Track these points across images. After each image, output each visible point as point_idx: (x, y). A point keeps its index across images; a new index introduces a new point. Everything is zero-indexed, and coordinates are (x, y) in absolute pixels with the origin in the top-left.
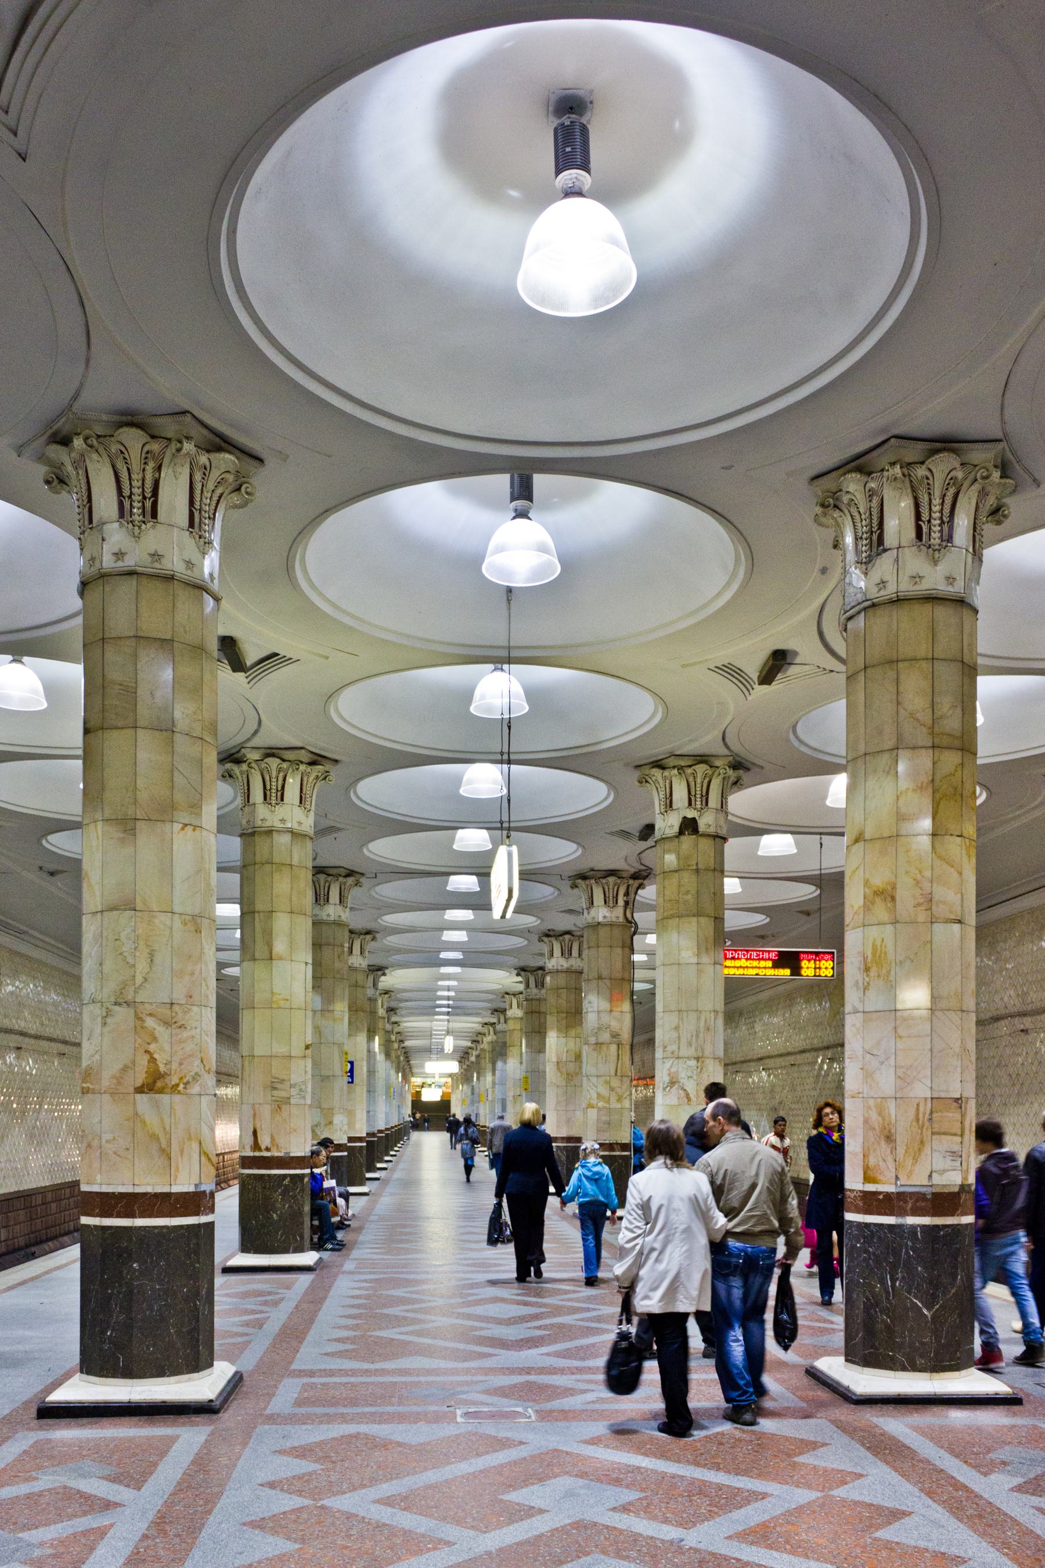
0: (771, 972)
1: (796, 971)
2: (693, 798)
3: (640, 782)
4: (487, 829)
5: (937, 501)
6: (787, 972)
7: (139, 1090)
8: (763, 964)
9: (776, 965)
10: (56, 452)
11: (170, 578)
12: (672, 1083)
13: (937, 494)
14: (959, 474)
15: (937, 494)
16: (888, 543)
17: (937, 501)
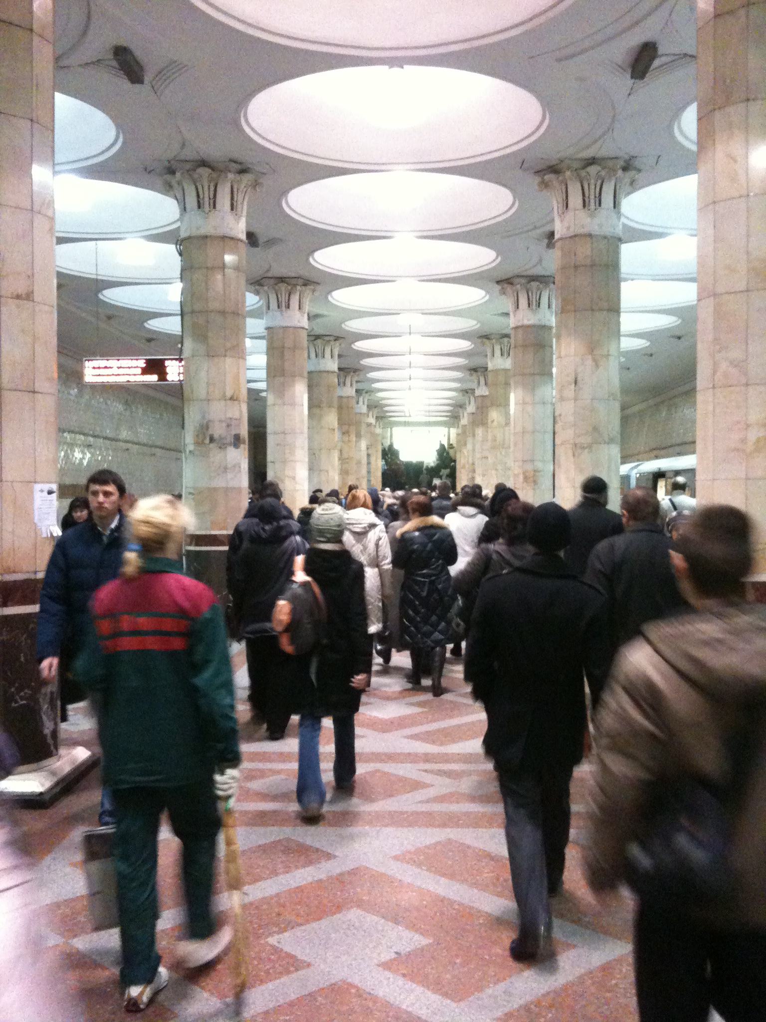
2: (587, 200)
5: (592, 187)
10: (168, 177)
14: (603, 173)
17: (592, 187)
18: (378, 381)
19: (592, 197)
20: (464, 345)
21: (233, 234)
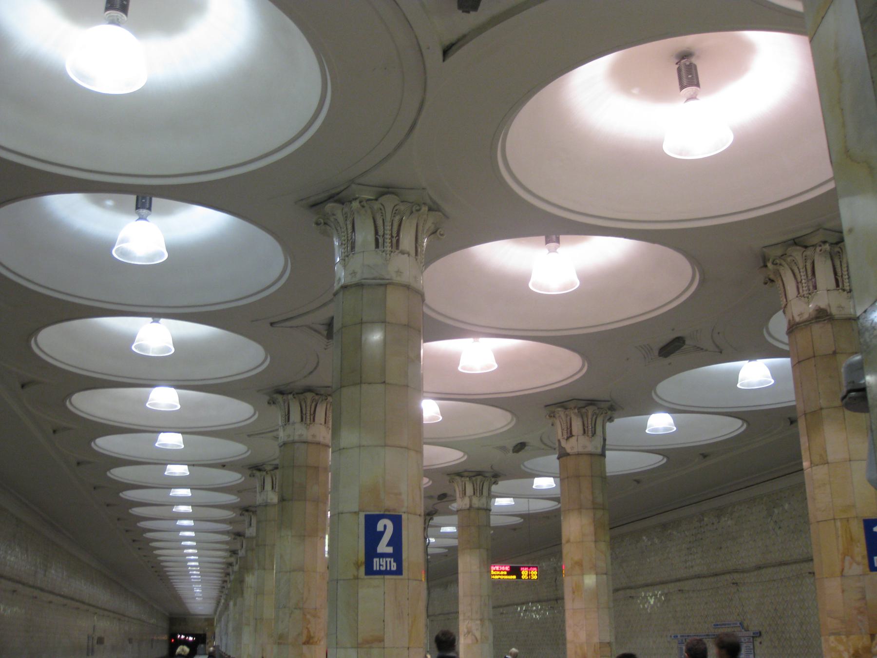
0: (506, 577)
1: (519, 576)
3: (269, 403)
4: (182, 433)
6: (514, 577)
7: (304, 644)
8: (502, 573)
9: (509, 573)
11: (318, 443)
12: (469, 632)
13: (590, 417)
14: (597, 411)
15: (590, 417)
16: (574, 433)
18: (166, 561)
19: (308, 415)
20: (232, 477)
21: (321, 440)
